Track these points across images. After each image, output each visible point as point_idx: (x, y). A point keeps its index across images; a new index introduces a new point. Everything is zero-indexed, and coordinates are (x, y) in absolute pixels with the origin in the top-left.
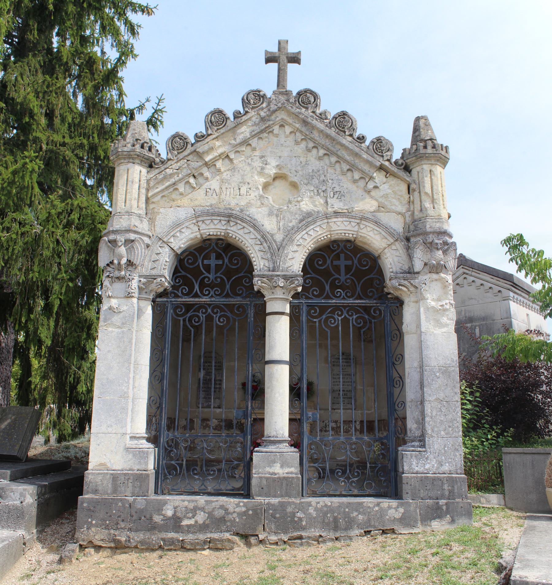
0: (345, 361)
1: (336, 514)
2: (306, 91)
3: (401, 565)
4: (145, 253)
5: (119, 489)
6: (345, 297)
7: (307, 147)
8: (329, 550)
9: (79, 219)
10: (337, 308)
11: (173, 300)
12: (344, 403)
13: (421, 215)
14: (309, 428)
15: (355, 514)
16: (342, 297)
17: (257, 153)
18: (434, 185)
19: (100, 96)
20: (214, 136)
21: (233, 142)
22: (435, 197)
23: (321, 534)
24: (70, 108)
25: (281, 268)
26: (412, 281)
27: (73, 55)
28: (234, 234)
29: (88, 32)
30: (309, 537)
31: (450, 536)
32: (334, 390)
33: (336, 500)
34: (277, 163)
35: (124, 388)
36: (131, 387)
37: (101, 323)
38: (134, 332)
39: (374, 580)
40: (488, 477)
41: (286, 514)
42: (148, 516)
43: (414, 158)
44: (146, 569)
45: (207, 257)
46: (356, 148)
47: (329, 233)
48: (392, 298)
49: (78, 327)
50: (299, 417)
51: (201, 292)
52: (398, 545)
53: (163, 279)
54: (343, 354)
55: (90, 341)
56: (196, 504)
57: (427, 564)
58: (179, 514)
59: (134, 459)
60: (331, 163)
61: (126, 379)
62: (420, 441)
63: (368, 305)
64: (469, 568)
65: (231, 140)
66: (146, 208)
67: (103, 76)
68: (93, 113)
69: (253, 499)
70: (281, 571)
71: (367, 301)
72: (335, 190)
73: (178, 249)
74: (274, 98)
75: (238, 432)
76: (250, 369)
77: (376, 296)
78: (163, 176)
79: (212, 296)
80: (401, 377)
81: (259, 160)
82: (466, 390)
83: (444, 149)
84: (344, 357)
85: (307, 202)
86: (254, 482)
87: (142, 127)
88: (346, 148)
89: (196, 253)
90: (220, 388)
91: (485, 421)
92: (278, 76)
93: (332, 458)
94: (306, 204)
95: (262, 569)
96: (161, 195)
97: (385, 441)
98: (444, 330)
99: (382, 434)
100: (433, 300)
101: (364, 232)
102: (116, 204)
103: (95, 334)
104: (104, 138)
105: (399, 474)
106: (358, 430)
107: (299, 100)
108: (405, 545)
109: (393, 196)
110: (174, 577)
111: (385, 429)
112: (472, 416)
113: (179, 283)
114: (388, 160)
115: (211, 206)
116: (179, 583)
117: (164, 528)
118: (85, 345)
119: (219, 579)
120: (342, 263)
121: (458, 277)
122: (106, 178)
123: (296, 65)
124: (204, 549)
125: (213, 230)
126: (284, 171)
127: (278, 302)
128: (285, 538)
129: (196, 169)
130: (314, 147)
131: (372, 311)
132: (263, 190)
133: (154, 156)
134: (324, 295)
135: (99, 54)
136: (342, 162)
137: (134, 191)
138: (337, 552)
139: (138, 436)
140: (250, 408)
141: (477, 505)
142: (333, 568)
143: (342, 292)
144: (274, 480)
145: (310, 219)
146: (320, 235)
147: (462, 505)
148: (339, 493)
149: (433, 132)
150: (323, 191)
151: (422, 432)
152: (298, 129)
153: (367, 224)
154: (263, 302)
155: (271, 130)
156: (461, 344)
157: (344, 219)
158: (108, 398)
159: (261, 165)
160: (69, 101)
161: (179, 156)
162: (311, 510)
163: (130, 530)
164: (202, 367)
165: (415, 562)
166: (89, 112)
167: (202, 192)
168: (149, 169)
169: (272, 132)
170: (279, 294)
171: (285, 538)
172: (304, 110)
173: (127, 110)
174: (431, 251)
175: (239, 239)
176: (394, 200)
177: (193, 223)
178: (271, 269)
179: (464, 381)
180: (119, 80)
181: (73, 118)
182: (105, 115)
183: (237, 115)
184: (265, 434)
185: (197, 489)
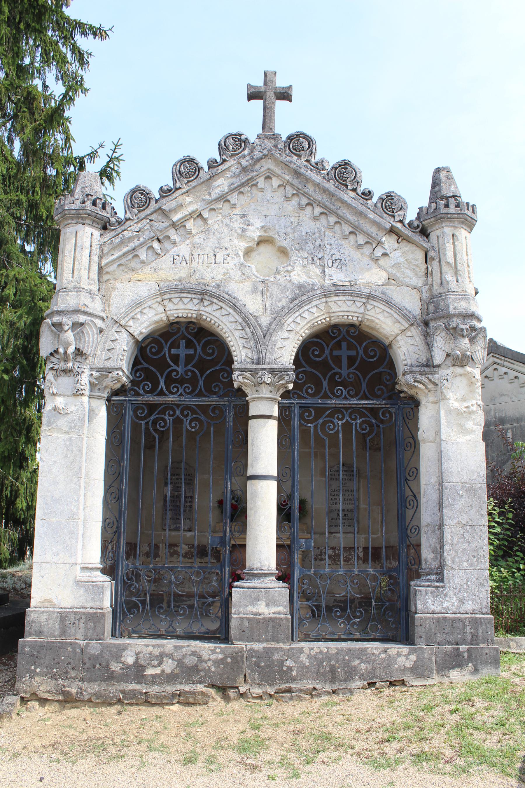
0: (345, 473)
1: (333, 663)
2: (299, 135)
3: (413, 724)
4: (97, 339)
5: (69, 631)
6: (348, 396)
7: (299, 204)
8: (324, 705)
9: (15, 295)
10: (337, 410)
11: (132, 399)
12: (344, 526)
13: (441, 290)
14: (300, 556)
15: (357, 662)
16: (343, 396)
17: (237, 211)
18: (457, 252)
19: (41, 141)
20: (183, 191)
21: (207, 197)
22: (459, 268)
23: (315, 686)
24: (4, 156)
25: (267, 360)
26: (431, 377)
27: (7, 89)
28: (209, 316)
29: (27, 61)
30: (300, 690)
31: (472, 690)
32: (331, 510)
33: (334, 646)
34: (262, 224)
35: (72, 508)
36: (82, 507)
37: (44, 427)
38: (85, 439)
39: (379, 743)
40: (519, 616)
41: (273, 662)
42: (104, 664)
43: (433, 219)
44: (103, 727)
45: (175, 345)
46: (360, 206)
47: (327, 315)
48: (405, 397)
49: (15, 430)
50: (289, 543)
51: (168, 387)
52: (409, 700)
53: (121, 373)
54: (343, 465)
55: (29, 445)
56: (162, 650)
57: (444, 724)
58: (142, 662)
59: (87, 595)
60: (329, 224)
61: (75, 497)
62: (437, 574)
63: (376, 406)
64: (496, 730)
65: (205, 195)
66: (99, 280)
67: (45, 116)
68: (33, 162)
69: (233, 644)
70: (266, 731)
71: (375, 401)
72: (334, 257)
73: (139, 335)
74: (259, 143)
75: (213, 561)
76: (229, 485)
77: (386, 395)
78: (119, 240)
79: (181, 395)
80: (415, 496)
81: (239, 220)
82: (495, 510)
83: (470, 208)
84: (345, 469)
85: (300, 273)
86: (233, 623)
87: (94, 179)
88: (348, 206)
89: (161, 339)
90: (191, 507)
91: (517, 548)
92: (264, 116)
93: (330, 593)
94: (298, 275)
95: (242, 729)
96: (117, 264)
97: (394, 574)
98: (470, 437)
99: (391, 563)
100: (457, 400)
101: (372, 314)
102: (62, 274)
103: (36, 438)
104: (46, 194)
105: (411, 614)
106: (361, 559)
107: (289, 145)
108: (418, 700)
109: (407, 266)
110: (137, 737)
111: (394, 558)
112: (502, 543)
113: (139, 377)
114: (401, 221)
115: (180, 280)
116: (143, 745)
117: (124, 678)
118: (23, 452)
119: (191, 740)
120: (344, 353)
121: (487, 368)
122: (49, 243)
123: (286, 102)
124: (173, 704)
125: (183, 311)
126: (271, 234)
127: (264, 402)
128: (271, 691)
129: (161, 231)
130: (308, 204)
131: (380, 414)
132: (244, 257)
133: (109, 216)
134: (321, 394)
135: (40, 89)
136: (343, 223)
137: (84, 258)
138: (334, 708)
139: (90, 566)
140: (228, 534)
141: (505, 650)
142: (330, 728)
143: (344, 390)
144: (258, 621)
145: (304, 298)
146: (317, 317)
147: (487, 652)
148: (337, 637)
149: (457, 187)
150: (320, 259)
151: (440, 563)
152: (288, 181)
153: (375, 304)
154: (245, 403)
155: (254, 182)
156: (489, 451)
157: (347, 298)
158: (54, 519)
159: (242, 226)
160: (3, 148)
161: (139, 215)
162: (303, 658)
163: (82, 680)
164: (169, 481)
165: (429, 720)
166: (28, 160)
167: (168, 259)
168: (103, 231)
169: (255, 185)
170: (265, 392)
171: (271, 691)
172: (295, 158)
173: (76, 158)
174: (455, 338)
175: (215, 322)
176: (408, 271)
177: (157, 302)
178: (255, 361)
179: (491, 499)
180: (65, 121)
181: (8, 169)
182: (48, 164)
183: (212, 164)
184: (247, 565)
185: (163, 631)
